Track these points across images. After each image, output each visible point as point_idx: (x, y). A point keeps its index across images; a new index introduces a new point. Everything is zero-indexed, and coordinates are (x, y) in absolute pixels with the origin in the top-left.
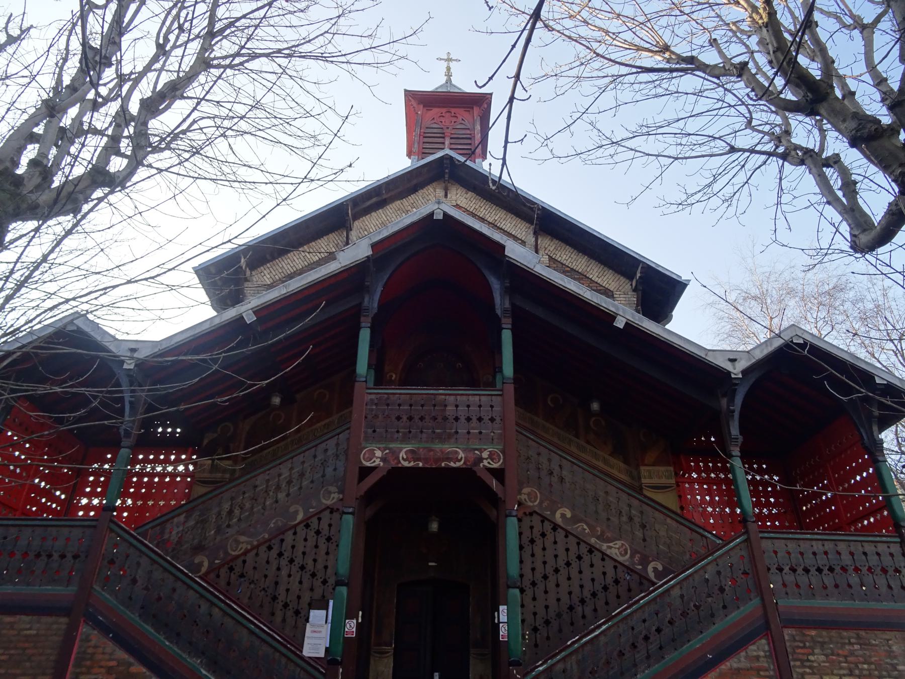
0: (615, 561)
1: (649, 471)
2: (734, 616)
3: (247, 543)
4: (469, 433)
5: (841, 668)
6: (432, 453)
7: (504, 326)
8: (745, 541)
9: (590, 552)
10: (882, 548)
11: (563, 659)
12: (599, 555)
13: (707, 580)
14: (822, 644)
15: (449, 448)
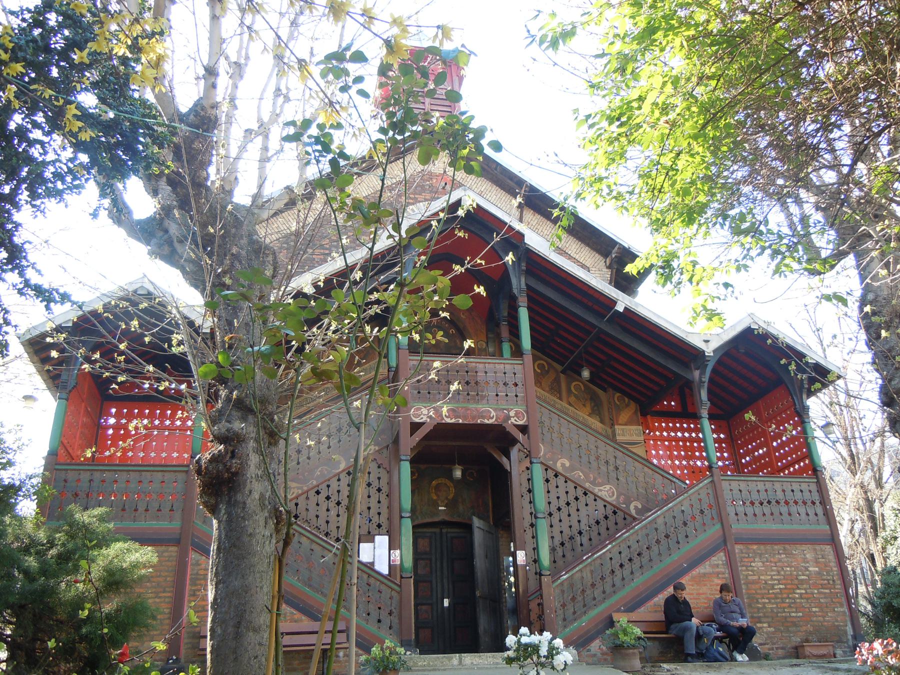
0: (605, 501)
1: (623, 430)
2: (702, 537)
3: (298, 488)
4: (497, 395)
5: (772, 571)
6: (469, 412)
7: (520, 304)
8: (711, 482)
9: (585, 494)
10: (804, 487)
11: (581, 570)
12: (592, 497)
13: (683, 511)
14: (761, 555)
15: (482, 407)
